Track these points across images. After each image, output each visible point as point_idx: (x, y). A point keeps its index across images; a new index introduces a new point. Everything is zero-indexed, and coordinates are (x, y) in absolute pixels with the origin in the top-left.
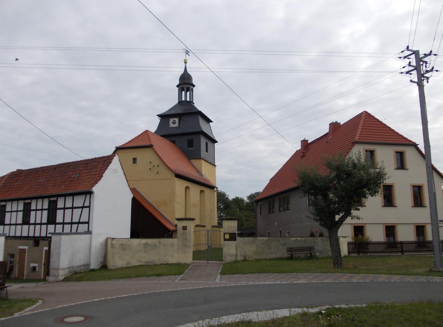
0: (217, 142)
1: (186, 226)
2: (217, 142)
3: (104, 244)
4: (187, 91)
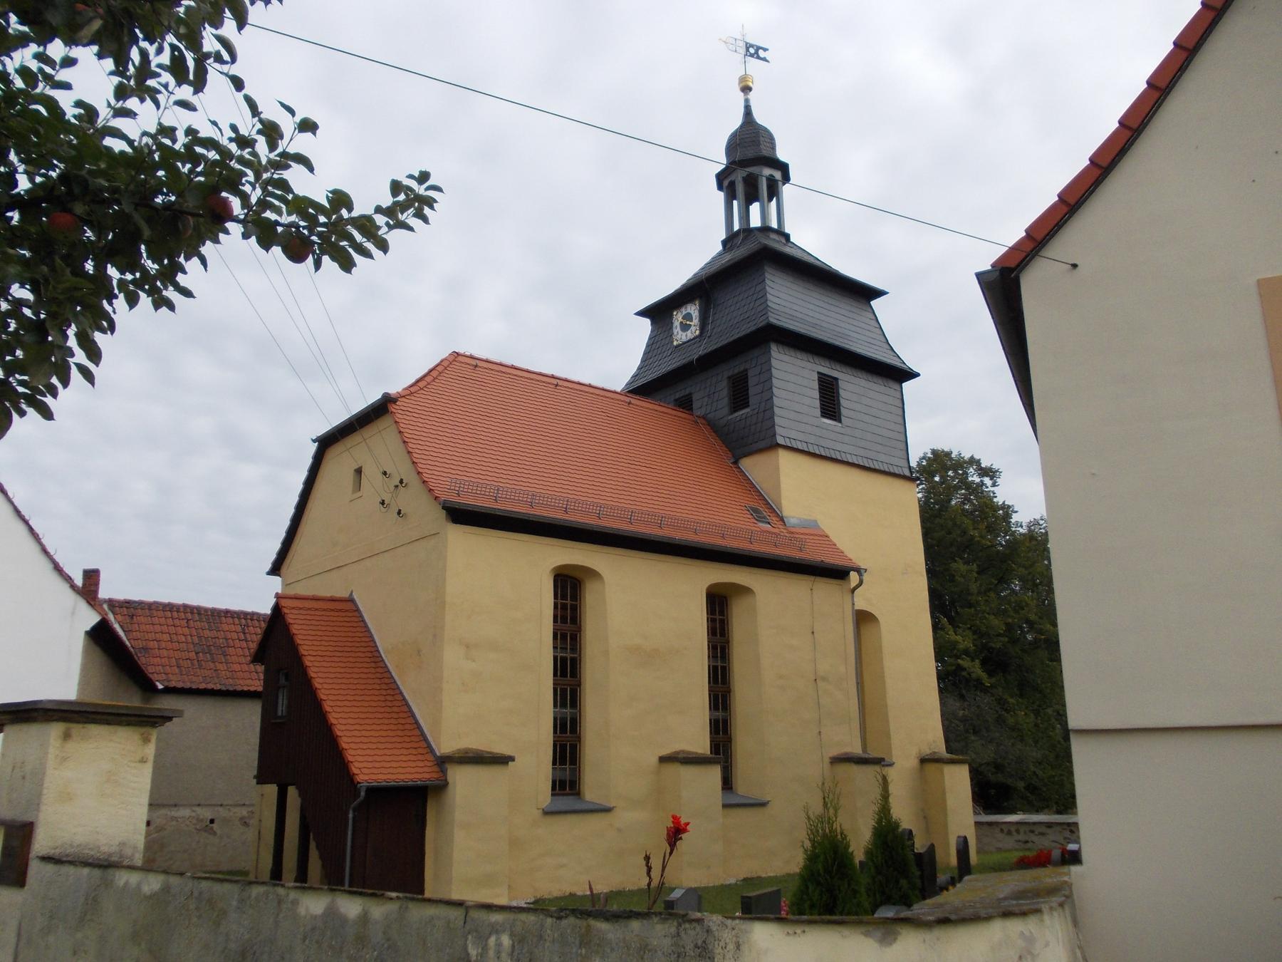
0: (916, 375)
1: (1260, 283)
2: (916, 375)
3: (878, 934)
4: (770, 200)
